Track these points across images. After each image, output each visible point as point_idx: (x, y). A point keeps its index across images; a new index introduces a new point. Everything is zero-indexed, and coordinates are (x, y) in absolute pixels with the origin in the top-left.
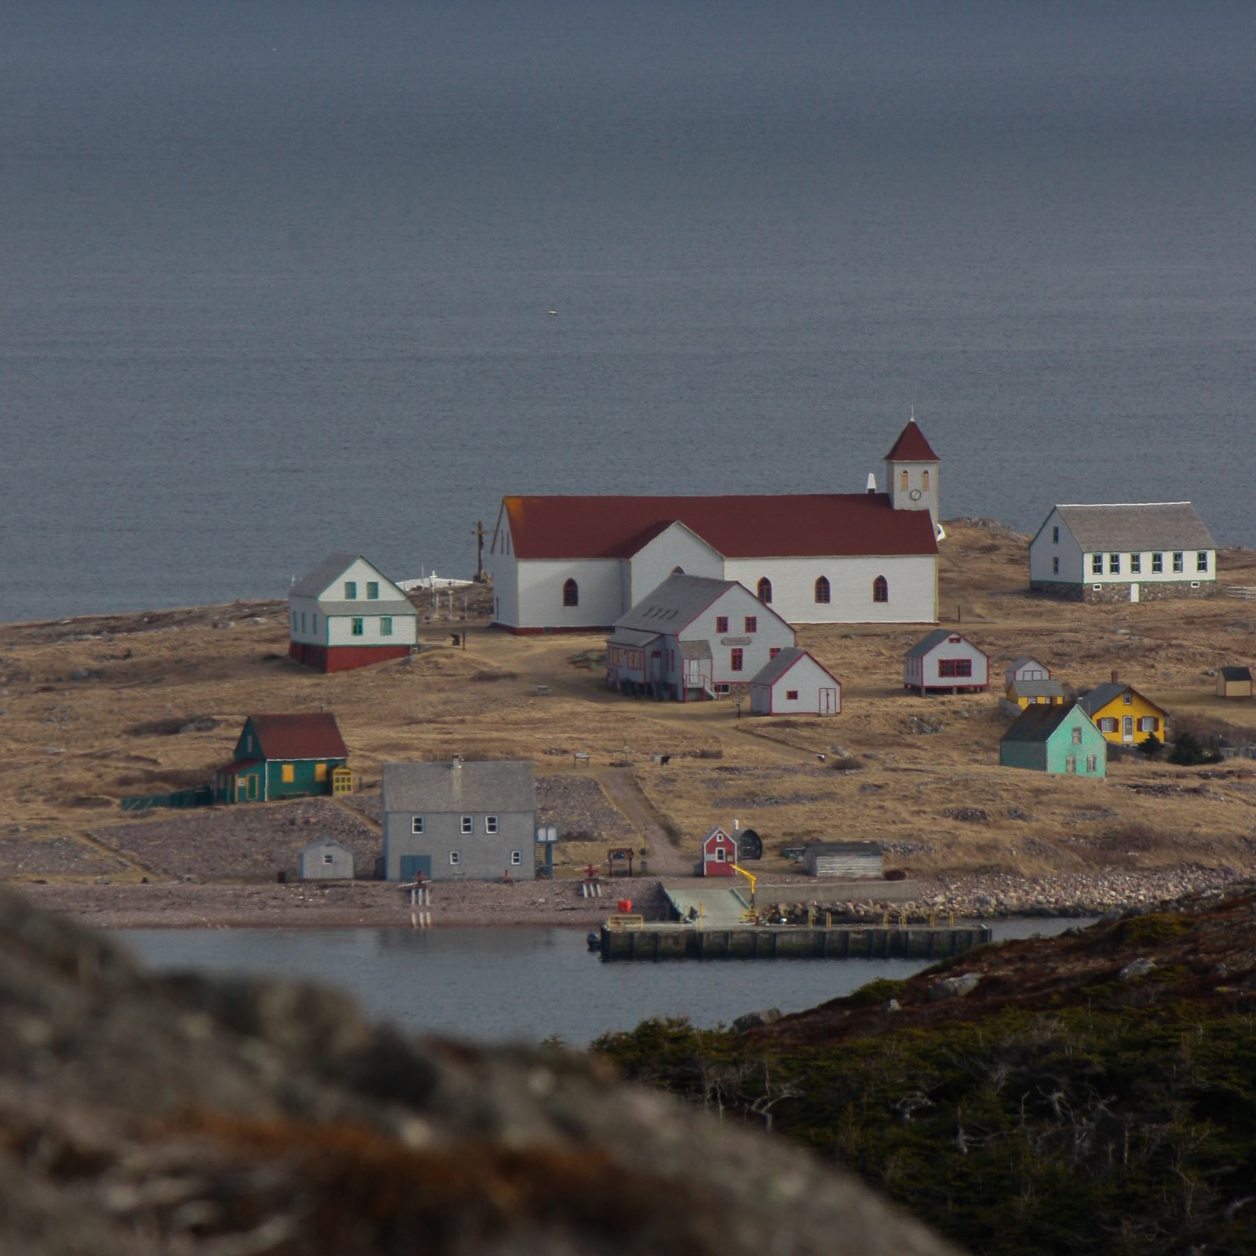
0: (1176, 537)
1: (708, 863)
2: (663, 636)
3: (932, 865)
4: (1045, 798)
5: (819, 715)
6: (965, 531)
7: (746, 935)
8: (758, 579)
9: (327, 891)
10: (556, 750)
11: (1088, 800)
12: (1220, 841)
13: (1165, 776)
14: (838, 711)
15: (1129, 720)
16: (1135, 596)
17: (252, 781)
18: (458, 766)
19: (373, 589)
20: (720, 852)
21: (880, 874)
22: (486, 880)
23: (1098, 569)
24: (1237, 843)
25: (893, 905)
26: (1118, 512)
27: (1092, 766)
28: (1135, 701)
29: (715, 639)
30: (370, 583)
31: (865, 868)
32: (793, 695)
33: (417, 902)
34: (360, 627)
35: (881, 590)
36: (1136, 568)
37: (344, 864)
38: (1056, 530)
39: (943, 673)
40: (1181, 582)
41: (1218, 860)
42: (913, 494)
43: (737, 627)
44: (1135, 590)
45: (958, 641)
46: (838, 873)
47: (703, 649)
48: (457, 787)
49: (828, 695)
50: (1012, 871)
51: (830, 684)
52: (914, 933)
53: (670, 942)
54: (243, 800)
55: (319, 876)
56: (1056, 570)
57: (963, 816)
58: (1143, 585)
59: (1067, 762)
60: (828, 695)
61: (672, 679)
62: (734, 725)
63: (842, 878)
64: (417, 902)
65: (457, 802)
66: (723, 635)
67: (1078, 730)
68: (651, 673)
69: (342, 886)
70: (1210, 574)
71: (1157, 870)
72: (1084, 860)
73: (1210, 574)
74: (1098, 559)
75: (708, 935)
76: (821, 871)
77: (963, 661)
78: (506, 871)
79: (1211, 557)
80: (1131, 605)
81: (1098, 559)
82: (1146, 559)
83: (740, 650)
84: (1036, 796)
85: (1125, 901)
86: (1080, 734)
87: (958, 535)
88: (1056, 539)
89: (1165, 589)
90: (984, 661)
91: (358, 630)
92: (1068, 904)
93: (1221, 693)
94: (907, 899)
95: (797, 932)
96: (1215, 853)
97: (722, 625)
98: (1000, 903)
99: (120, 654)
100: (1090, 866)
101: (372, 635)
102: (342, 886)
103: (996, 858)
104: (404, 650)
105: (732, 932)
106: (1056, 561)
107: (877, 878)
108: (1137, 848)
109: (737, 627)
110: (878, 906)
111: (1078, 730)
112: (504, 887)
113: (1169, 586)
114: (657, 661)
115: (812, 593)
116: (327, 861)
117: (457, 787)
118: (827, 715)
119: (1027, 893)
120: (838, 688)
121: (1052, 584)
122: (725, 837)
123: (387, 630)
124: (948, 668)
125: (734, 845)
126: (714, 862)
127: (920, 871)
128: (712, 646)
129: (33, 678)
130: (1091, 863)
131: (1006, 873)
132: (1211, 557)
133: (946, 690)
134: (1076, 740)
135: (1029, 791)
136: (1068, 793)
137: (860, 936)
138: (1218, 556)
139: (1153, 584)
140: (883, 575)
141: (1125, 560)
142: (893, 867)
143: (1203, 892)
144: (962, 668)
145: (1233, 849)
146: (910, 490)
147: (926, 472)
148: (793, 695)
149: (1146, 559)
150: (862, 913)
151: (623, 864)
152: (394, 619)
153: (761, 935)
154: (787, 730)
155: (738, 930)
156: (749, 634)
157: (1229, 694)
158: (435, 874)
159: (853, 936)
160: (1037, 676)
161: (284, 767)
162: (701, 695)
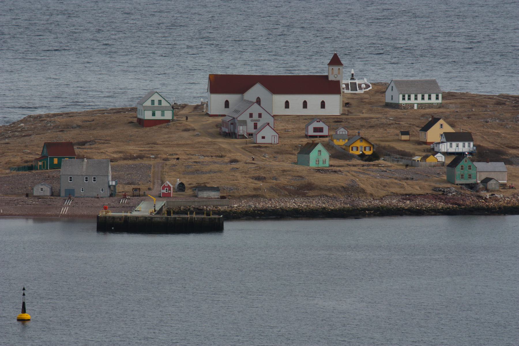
0: (430, 89)
1: (162, 193)
2: (234, 118)
3: (238, 194)
4: (285, 173)
5: (271, 144)
6: (378, 87)
7: (143, 218)
8: (285, 101)
9: (40, 200)
10: (174, 154)
11: (300, 174)
12: (335, 188)
13: (335, 166)
14: (278, 142)
15: (361, 147)
16: (416, 107)
17: (44, 163)
18: (85, 160)
19: (160, 102)
20: (166, 189)
21: (219, 197)
22: (92, 197)
23: (404, 99)
24: (340, 189)
25: (220, 207)
27: (324, 162)
28: (363, 141)
29: (249, 120)
30: (159, 100)
31: (214, 195)
32: (263, 138)
33: (66, 204)
34: (155, 114)
35: (323, 105)
36: (416, 99)
37: (47, 191)
38: (392, 87)
39: (314, 132)
40: (431, 103)
41: (333, 194)
42: (335, 76)
43: (255, 116)
45: (319, 122)
46: (205, 196)
47: (244, 123)
48: (85, 167)
49: (274, 138)
50: (264, 197)
51: (275, 134)
52: (197, 218)
53: (118, 220)
54: (40, 169)
55: (39, 194)
56: (392, 99)
57: (258, 178)
58: (418, 104)
59: (316, 161)
60: (274, 138)
61: (236, 132)
62: (242, 147)
63: (206, 198)
64: (66, 204)
65: (84, 172)
66: (251, 119)
67: (320, 151)
68: (230, 130)
69: (45, 198)
70: (440, 101)
71: (313, 196)
72: (289, 193)
73: (440, 101)
74: (404, 96)
75: (131, 217)
76: (200, 196)
77: (321, 128)
78: (98, 195)
79: (440, 96)
80: (415, 110)
81: (404, 96)
82: (419, 96)
83: (257, 123)
84: (283, 173)
85: (297, 207)
86: (321, 152)
88: (392, 90)
89: (425, 105)
90: (327, 127)
91: (154, 114)
92: (278, 207)
93: (400, 139)
94: (224, 206)
95: (159, 217)
96: (332, 192)
97: (251, 115)
98: (255, 207)
99: (91, 120)
100: (290, 195)
101: (158, 116)
102: (45, 198)
104: (168, 121)
105: (138, 217)
106: (392, 96)
107: (218, 198)
108: (308, 190)
109: (255, 116)
110: (215, 207)
111: (320, 151)
112: (96, 199)
113: (426, 104)
114: (232, 126)
115: (223, 105)
116: (41, 190)
117: (85, 167)
118: (274, 144)
119: (266, 204)
120: (278, 135)
121: (391, 103)
122: (168, 185)
123: (163, 115)
124: (316, 130)
125: (171, 187)
126: (164, 193)
127: (234, 196)
128: (247, 122)
129: (60, 127)
130: (291, 194)
131: (261, 197)
132: (440, 96)
133: (316, 137)
134: (319, 154)
135: (282, 171)
136: (293, 172)
137: (180, 219)
138: (442, 96)
139: (421, 104)
140: (324, 100)
141: (413, 97)
142: (223, 195)
144: (321, 130)
145: (338, 190)
146: (334, 74)
147: (339, 69)
148: (263, 138)
149: (419, 96)
150: (208, 210)
151: (137, 193)
152: (165, 112)
153: (148, 218)
154: (257, 149)
155: (141, 216)
156: (259, 119)
157: (402, 139)
158: (76, 195)
159: (177, 218)
160: (344, 133)
161: (54, 159)
162: (243, 137)
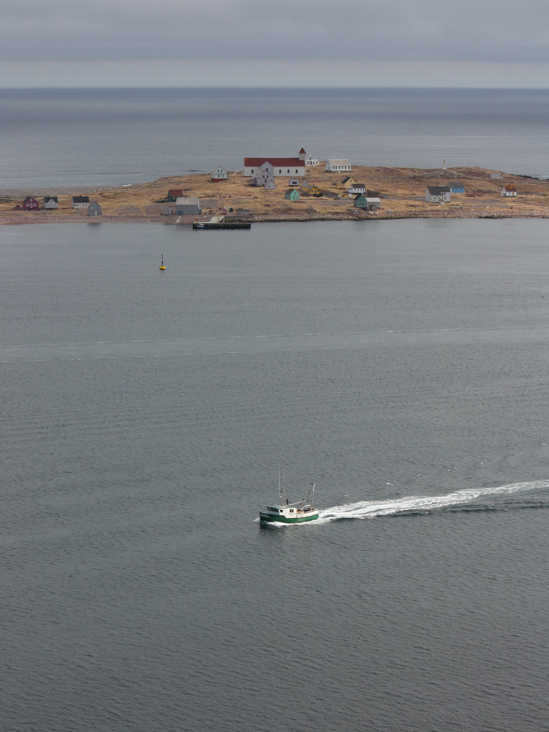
26: (337, 161)
32: (269, 187)
43: (266, 177)
44: (339, 172)
58: (340, 171)
61: (257, 184)
67: (295, 193)
87: (321, 163)
91: (219, 176)
97: (264, 176)
103: (268, 212)
109: (266, 177)
111: (295, 193)
143: (393, 190)
144: (296, 183)
145: (304, 211)
148: (269, 187)
